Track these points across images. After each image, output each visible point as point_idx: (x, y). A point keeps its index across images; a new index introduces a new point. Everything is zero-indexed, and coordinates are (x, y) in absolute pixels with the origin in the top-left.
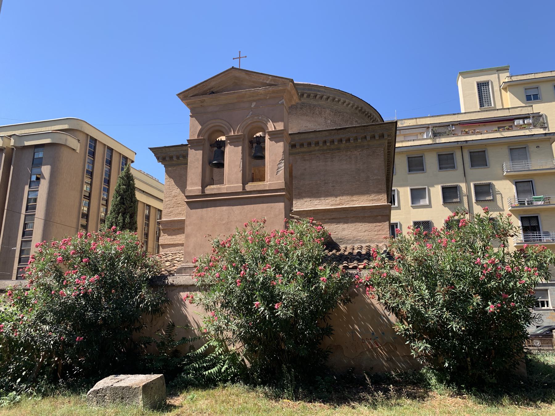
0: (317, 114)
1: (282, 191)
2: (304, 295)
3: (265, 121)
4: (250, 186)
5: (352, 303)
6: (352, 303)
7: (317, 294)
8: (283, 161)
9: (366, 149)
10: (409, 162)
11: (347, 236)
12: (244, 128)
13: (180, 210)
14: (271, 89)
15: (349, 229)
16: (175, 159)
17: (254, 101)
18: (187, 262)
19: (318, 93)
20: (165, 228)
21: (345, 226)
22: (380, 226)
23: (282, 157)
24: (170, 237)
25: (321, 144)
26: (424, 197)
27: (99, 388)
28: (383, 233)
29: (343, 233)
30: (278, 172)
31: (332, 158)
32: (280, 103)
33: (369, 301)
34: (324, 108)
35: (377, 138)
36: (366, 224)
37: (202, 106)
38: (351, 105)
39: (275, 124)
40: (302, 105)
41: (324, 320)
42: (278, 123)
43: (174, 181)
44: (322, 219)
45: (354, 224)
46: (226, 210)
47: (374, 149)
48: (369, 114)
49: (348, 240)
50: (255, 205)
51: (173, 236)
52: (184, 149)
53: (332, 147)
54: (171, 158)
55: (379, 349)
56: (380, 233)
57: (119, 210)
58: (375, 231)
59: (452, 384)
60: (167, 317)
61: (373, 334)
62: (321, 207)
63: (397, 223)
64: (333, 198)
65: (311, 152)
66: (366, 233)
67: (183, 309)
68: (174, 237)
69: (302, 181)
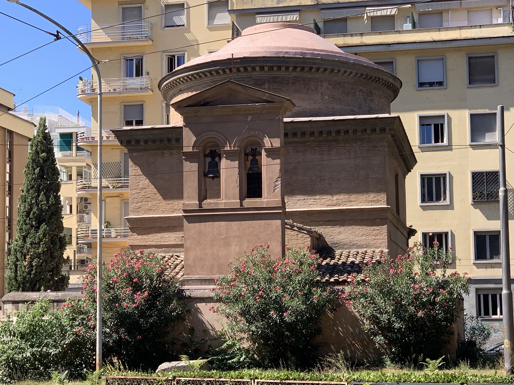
0: (312, 89)
1: (279, 208)
2: (303, 307)
3: (261, 136)
4: (249, 202)
5: (337, 312)
6: (337, 312)
7: (312, 307)
8: (280, 179)
9: (367, 142)
10: (470, 65)
11: (343, 241)
12: (241, 141)
13: (150, 205)
14: (267, 105)
15: (345, 233)
16: (142, 143)
17: (250, 114)
18: (188, 274)
19: (314, 66)
20: (134, 226)
21: (342, 229)
22: (378, 230)
23: (279, 175)
24: (140, 237)
25: (316, 134)
26: (492, 129)
27: (166, 368)
28: (381, 238)
29: (339, 237)
30: (275, 190)
31: (329, 151)
32: (276, 118)
33: (350, 310)
34: (320, 82)
35: (378, 131)
36: (364, 227)
37: (195, 115)
38: (354, 74)
39: (271, 140)
40: (295, 80)
41: (316, 324)
42: (274, 139)
43: (141, 170)
44: (317, 221)
45: (351, 227)
46: (224, 225)
47: (375, 142)
48: (377, 79)
49: (344, 245)
50: (253, 221)
51: (144, 236)
52: (153, 133)
53: (330, 138)
54: (138, 141)
55: (356, 344)
56: (378, 237)
57: (39, 186)
58: (373, 236)
59: (399, 363)
60: (187, 323)
61: (352, 333)
62: (316, 207)
63: (446, 174)
64: (329, 197)
65: (305, 142)
66: (364, 238)
67: (200, 316)
68: (145, 237)
69: (295, 176)
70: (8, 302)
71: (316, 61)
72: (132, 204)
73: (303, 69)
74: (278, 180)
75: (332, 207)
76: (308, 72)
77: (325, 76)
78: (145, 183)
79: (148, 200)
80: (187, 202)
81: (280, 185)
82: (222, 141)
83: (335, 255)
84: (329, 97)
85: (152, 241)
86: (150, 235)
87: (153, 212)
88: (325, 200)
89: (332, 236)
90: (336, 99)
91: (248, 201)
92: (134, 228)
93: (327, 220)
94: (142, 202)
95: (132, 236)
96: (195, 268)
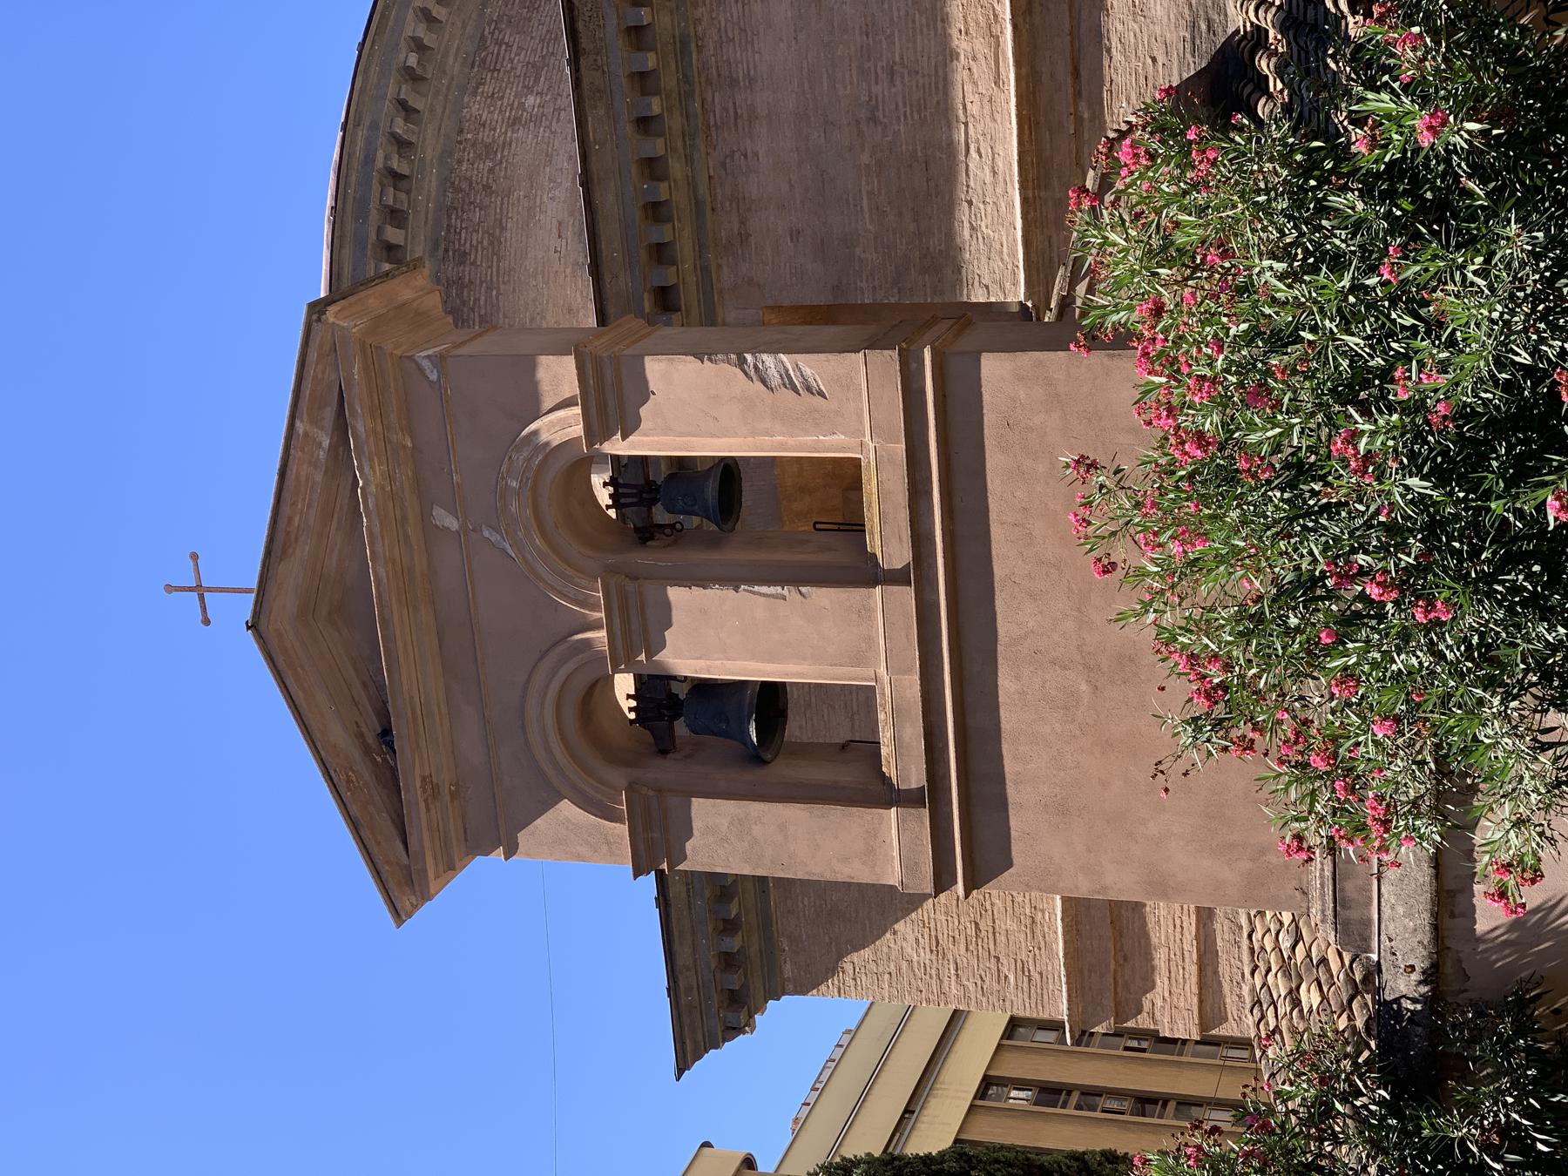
0: (491, 170)
1: (914, 366)
2: (1515, 239)
3: (529, 460)
8: (749, 357)
13: (1011, 925)
14: (360, 424)
16: (734, 943)
17: (425, 516)
19: (379, 163)
24: (1161, 982)
25: (657, 147)
30: (809, 389)
31: (734, 82)
34: (461, 131)
37: (453, 795)
39: (547, 405)
40: (446, 250)
43: (856, 949)
44: (1078, 134)
46: (1018, 678)
50: (993, 516)
53: (669, 81)
62: (1005, 140)
65: (698, 204)
68: (1160, 959)
69: (858, 251)
70: (1531, 693)
71: (359, 151)
72: (1008, 1003)
73: (395, 216)
74: (756, 367)
75: (1005, 59)
76: (408, 192)
77: (439, 111)
78: (911, 938)
79: (991, 930)
80: (893, 867)
81: (782, 356)
82: (570, 666)
83: (1248, 29)
84: (529, 89)
85: (1178, 929)
86: (1152, 934)
87: (1043, 911)
88: (969, 98)
89: (1155, 53)
90: (544, 57)
91: (877, 537)
92: (1117, 1004)
93: (1069, 80)
94: (998, 958)
95: (1157, 1014)
96: (1262, 852)
